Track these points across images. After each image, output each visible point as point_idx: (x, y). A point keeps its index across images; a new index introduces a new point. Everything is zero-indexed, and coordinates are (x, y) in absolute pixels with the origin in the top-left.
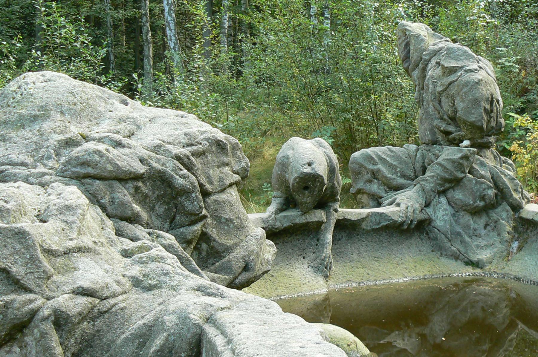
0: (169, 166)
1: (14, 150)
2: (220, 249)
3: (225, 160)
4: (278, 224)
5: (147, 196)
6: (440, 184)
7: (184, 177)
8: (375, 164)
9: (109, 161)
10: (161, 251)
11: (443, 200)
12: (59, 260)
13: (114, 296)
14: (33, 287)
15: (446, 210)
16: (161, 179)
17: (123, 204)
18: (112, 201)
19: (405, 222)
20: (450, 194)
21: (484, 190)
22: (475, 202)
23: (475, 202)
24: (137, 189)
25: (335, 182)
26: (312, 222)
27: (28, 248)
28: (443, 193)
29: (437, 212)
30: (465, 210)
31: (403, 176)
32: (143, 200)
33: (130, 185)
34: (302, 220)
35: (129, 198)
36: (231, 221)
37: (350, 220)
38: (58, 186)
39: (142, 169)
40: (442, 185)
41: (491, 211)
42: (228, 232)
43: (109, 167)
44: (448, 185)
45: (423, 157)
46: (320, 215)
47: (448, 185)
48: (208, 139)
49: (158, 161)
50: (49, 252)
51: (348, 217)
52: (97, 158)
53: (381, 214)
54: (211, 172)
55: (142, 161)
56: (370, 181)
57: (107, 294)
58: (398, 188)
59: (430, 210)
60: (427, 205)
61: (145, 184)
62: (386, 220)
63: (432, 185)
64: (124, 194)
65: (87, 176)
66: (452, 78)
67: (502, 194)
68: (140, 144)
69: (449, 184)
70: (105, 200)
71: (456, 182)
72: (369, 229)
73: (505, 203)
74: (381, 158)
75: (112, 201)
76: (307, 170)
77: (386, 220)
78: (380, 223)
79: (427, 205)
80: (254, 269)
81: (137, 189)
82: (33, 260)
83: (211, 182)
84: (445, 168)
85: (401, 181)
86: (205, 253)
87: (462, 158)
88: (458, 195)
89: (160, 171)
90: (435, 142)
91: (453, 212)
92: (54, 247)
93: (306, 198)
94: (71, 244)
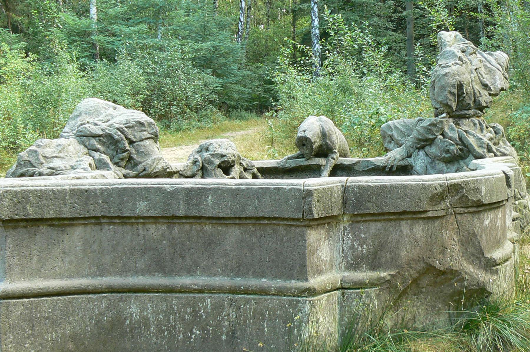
0: (113, 131)
1: (523, 119)
2: (138, 163)
3: (144, 129)
4: (287, 165)
5: (105, 142)
6: (416, 143)
7: (118, 136)
9: (88, 130)
11: (421, 153)
12: (49, 160)
13: (62, 170)
14: (36, 166)
15: (423, 159)
16: (109, 136)
17: (92, 145)
18: (89, 144)
19: (386, 166)
20: (427, 149)
21: (447, 146)
22: (441, 154)
23: (441, 154)
24: (100, 140)
25: (328, 141)
26: (313, 165)
27: (37, 155)
28: (422, 148)
29: (417, 161)
30: (438, 160)
32: (103, 144)
33: (97, 138)
34: (306, 163)
35: (96, 143)
36: (143, 152)
37: (344, 164)
39: (101, 133)
40: (418, 143)
41: (460, 161)
42: (142, 156)
43: (88, 133)
44: (422, 143)
46: (321, 161)
47: (422, 143)
48: (135, 121)
49: (109, 130)
50: (45, 157)
51: (343, 163)
52: (84, 129)
53: (368, 161)
54: (136, 134)
55: (102, 130)
56: (390, 142)
57: (59, 169)
59: (410, 160)
61: (104, 138)
62: (372, 165)
63: (411, 143)
64: (95, 142)
65: (81, 136)
70: (87, 144)
71: (430, 142)
72: (361, 170)
73: (471, 155)
74: (396, 127)
75: (89, 144)
77: (372, 165)
78: (368, 167)
79: (409, 156)
80: (148, 170)
81: (100, 140)
82: (38, 159)
83: (135, 138)
84: (419, 132)
87: (430, 125)
88: (433, 150)
89: (109, 134)
91: (430, 161)
92: (47, 156)
94: (54, 155)
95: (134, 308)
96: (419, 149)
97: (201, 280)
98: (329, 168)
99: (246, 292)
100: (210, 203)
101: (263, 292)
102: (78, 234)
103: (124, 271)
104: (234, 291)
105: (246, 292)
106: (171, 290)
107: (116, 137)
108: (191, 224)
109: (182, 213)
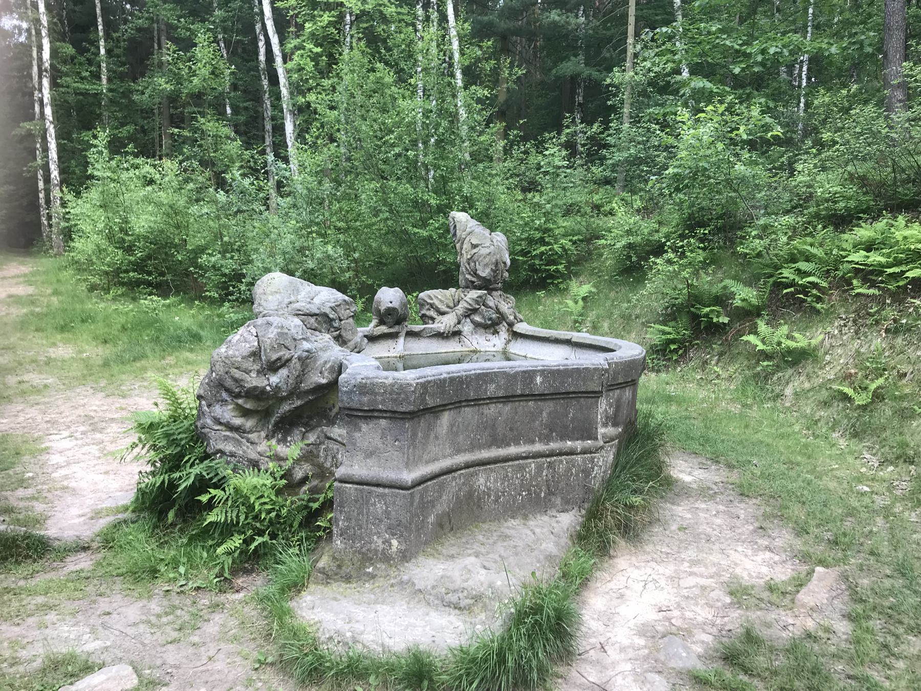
0: (328, 311)
8: (432, 299)
10: (326, 338)
11: (468, 320)
16: (325, 315)
20: (472, 317)
28: (468, 316)
31: (448, 307)
38: (290, 317)
39: (317, 312)
45: (459, 296)
56: (429, 309)
58: (443, 314)
59: (460, 326)
60: (459, 323)
66: (475, 251)
67: (502, 317)
68: (317, 301)
69: (469, 313)
71: (475, 311)
76: (390, 305)
79: (459, 323)
85: (448, 310)
86: (340, 340)
90: (467, 287)
93: (390, 320)
95: (482, 481)
96: (466, 317)
97: (523, 449)
98: (404, 333)
99: (561, 454)
100: (538, 382)
101: (572, 452)
102: (446, 418)
103: (472, 448)
104: (551, 454)
105: (561, 454)
106: (506, 459)
107: (331, 316)
108: (535, 400)
109: (519, 392)
